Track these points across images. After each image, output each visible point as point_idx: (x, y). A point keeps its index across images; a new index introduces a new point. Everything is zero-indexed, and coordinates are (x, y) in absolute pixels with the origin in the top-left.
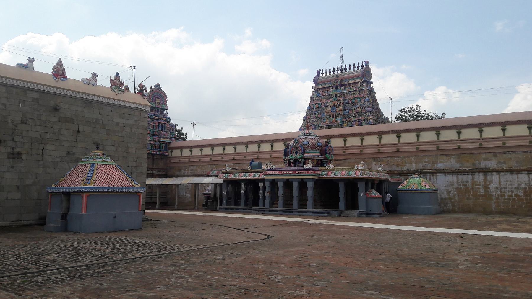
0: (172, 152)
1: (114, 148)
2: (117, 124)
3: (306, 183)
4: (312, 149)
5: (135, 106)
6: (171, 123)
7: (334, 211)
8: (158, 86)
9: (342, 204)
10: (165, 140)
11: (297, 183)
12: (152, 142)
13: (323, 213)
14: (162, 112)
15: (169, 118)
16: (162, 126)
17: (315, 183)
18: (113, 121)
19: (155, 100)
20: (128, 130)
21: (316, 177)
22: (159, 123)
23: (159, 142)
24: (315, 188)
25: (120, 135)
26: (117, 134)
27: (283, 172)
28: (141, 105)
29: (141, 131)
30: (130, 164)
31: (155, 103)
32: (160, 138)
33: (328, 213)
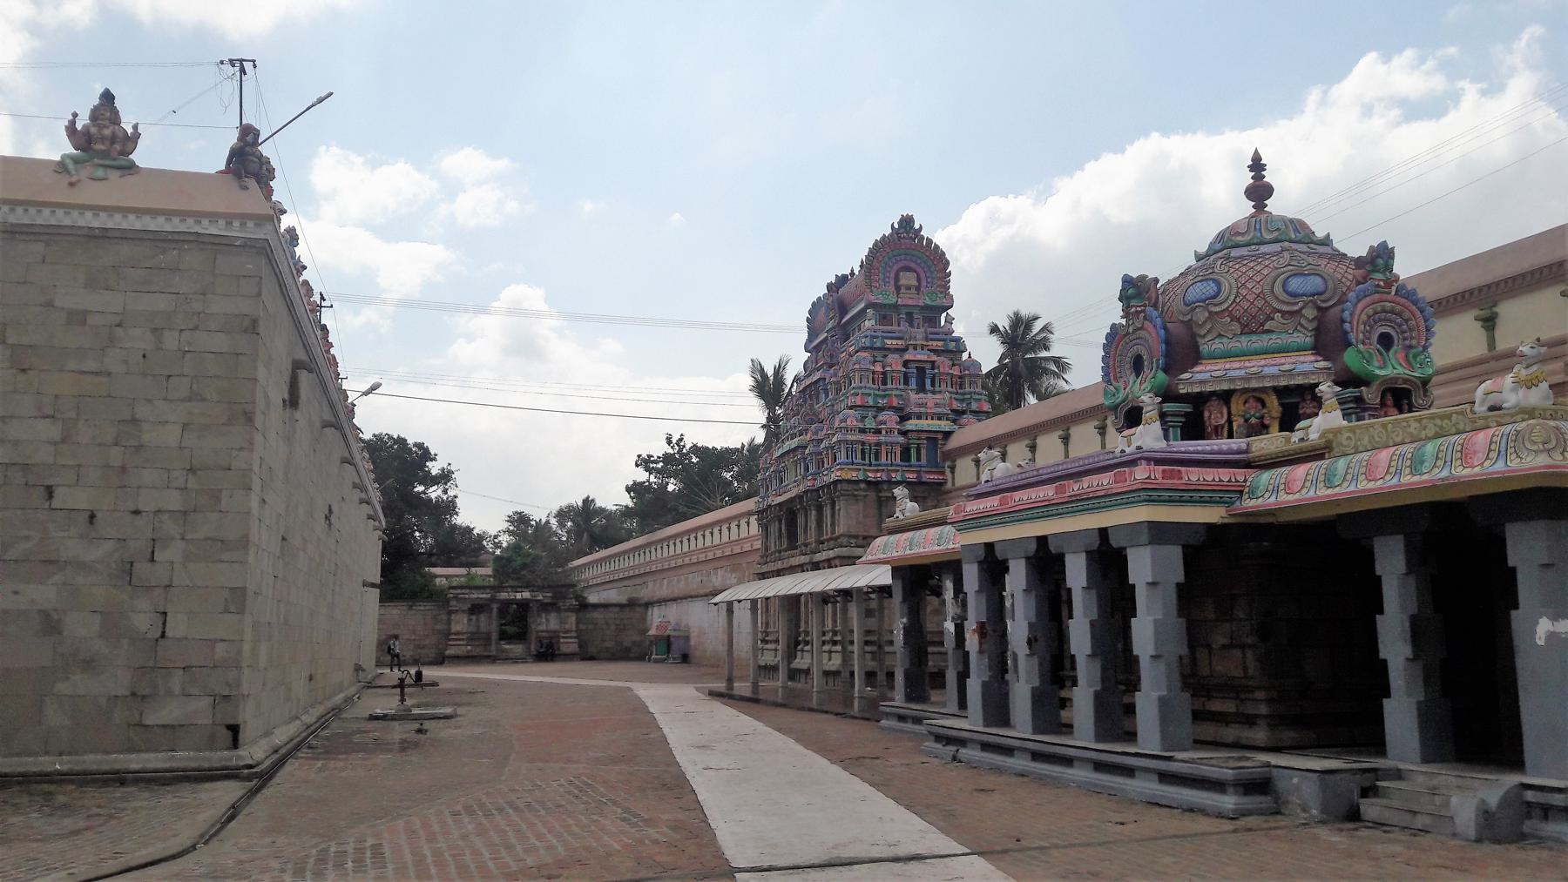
0: (953, 469)
1: (52, 431)
2: (78, 318)
3: (1060, 559)
4: (1252, 324)
5: (176, 225)
6: (965, 356)
7: (1302, 771)
8: (907, 222)
9: (1401, 715)
10: (924, 424)
11: (1023, 561)
12: (872, 438)
13: (1218, 786)
14: (933, 321)
15: (958, 340)
16: (921, 372)
17: (1192, 557)
18: (50, 304)
19: (897, 279)
20: (138, 339)
21: (1212, 515)
22: (906, 364)
23: (904, 433)
24: (1187, 596)
25: (90, 365)
26: (72, 365)
27: (1017, 495)
28: (213, 217)
29: (220, 342)
30: (147, 503)
31: (898, 288)
32: (904, 418)
33: (1259, 785)
